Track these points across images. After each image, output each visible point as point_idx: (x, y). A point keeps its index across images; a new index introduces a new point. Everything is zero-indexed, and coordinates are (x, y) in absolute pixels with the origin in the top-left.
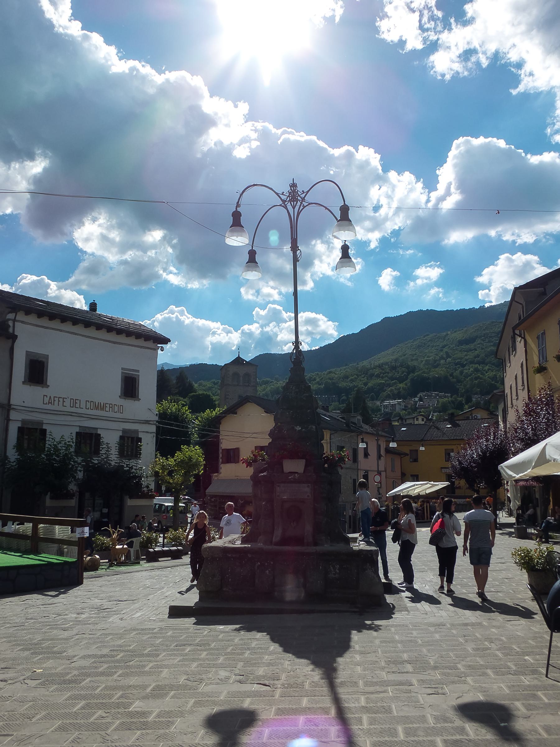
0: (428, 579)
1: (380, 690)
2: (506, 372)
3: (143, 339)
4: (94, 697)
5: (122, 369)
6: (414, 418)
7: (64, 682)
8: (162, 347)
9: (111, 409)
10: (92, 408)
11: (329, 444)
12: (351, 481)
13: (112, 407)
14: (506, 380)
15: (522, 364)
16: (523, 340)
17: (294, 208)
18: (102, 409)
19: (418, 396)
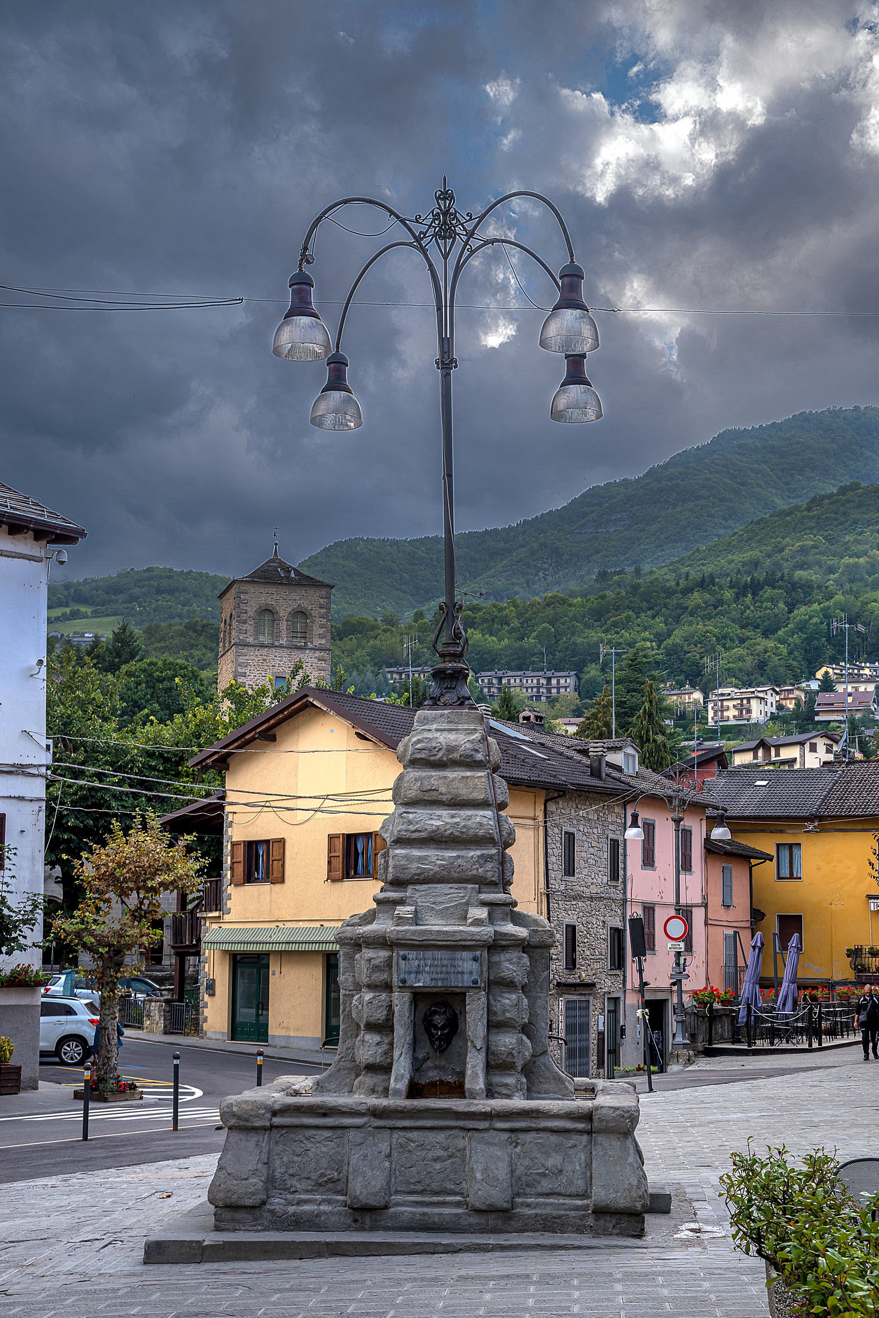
6: (802, 744)
11: (541, 829)
12: (604, 933)
17: (446, 256)
19: (819, 674)
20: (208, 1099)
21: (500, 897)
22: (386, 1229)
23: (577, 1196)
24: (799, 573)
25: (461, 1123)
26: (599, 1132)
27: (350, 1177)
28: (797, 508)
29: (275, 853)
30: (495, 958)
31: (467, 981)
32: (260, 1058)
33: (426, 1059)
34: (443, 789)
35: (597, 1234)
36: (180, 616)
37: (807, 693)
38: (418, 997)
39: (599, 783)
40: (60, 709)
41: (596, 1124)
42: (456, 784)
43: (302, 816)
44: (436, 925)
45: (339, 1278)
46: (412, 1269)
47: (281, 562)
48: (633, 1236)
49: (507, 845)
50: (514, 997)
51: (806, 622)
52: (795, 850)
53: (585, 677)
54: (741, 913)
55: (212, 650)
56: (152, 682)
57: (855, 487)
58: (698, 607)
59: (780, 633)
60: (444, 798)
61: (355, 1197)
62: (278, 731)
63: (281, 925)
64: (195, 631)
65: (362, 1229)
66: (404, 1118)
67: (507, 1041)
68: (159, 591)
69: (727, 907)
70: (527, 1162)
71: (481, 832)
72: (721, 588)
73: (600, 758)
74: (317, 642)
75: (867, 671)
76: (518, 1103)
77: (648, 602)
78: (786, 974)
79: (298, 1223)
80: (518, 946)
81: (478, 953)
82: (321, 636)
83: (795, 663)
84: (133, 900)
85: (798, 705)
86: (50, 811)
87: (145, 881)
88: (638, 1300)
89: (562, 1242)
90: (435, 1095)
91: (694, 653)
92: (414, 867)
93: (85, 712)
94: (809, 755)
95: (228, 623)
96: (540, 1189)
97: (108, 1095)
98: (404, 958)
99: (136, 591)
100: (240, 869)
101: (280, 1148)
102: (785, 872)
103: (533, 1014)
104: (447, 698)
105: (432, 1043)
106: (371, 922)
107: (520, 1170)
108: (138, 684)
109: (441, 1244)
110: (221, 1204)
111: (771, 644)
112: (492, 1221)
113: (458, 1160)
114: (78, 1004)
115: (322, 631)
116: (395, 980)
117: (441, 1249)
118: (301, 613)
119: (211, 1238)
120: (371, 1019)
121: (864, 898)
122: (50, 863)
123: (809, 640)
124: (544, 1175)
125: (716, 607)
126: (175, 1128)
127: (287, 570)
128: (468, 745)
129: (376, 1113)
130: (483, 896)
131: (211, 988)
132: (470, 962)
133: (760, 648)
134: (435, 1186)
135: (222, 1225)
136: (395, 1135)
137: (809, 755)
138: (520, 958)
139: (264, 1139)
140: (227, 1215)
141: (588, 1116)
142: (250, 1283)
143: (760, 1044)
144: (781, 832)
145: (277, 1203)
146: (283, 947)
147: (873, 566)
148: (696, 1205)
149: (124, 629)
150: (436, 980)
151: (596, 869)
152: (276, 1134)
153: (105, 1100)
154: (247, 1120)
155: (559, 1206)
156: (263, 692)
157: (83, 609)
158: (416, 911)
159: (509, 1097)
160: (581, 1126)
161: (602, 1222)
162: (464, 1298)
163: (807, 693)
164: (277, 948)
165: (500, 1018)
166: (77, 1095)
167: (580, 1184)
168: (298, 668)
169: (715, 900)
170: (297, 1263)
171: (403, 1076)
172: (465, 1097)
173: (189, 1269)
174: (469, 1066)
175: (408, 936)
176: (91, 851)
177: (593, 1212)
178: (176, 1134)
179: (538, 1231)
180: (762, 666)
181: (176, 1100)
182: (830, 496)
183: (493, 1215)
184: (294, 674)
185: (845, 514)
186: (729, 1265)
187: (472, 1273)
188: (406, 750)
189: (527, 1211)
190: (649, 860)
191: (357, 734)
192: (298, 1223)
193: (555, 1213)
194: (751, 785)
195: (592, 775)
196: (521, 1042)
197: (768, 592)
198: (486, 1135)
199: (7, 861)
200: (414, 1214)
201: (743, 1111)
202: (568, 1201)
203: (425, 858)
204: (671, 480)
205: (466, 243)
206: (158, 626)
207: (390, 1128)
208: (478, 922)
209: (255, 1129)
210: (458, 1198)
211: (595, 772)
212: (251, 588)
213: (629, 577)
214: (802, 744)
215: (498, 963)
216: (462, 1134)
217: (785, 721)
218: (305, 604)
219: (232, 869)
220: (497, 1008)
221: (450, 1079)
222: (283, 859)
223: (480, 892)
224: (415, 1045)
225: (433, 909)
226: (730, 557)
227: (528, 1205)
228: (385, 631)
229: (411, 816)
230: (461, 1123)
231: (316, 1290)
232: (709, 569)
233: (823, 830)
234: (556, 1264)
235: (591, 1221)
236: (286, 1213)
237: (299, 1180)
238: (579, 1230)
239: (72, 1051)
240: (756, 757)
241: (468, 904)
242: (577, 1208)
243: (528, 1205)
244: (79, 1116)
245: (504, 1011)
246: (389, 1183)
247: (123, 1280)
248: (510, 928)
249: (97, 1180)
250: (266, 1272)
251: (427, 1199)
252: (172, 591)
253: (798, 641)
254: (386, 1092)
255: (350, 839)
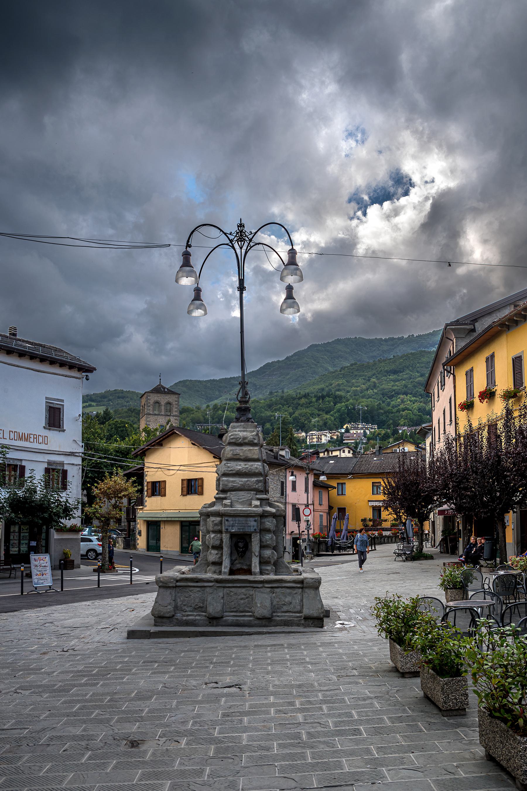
0: (363, 604)
1: (333, 688)
2: (434, 407)
3: (67, 367)
4: (86, 701)
5: (47, 398)
6: (340, 450)
7: (55, 691)
8: (87, 376)
9: (35, 440)
10: (16, 439)
13: (36, 438)
14: (434, 414)
15: (450, 399)
16: (452, 376)
17: (241, 248)
18: (26, 440)
19: (345, 427)
20: (141, 572)
21: (264, 496)
22: (222, 626)
23: (297, 612)
24: (337, 393)
25: (251, 585)
26: (306, 588)
27: (208, 606)
28: (336, 371)
29: (162, 485)
30: (263, 521)
31: (252, 529)
32: (161, 558)
33: (235, 560)
34: (241, 454)
35: (305, 626)
36: (126, 406)
37: (340, 433)
38: (233, 536)
39: (278, 462)
40: (86, 435)
41: (305, 585)
42: (247, 452)
43: (172, 472)
44: (239, 508)
45: (206, 646)
46: (235, 642)
47: (162, 386)
48: (320, 627)
49: (267, 476)
50: (270, 535)
51: (340, 409)
52: (344, 486)
53: (265, 428)
54: (325, 507)
55: (137, 418)
56: (117, 428)
57: (355, 364)
58: (304, 404)
59: (331, 413)
60: (242, 458)
61: (210, 614)
62: (163, 442)
63: (165, 511)
64: (131, 411)
65: (213, 626)
66: (229, 583)
67: (268, 553)
68: (119, 397)
69: (320, 505)
70: (278, 600)
71: (257, 471)
72: (311, 397)
73: (277, 453)
74: (175, 413)
75: (360, 426)
76: (272, 577)
77: (287, 402)
78: (344, 528)
79: (187, 623)
80: (272, 516)
81: (256, 518)
82: (176, 411)
83: (336, 423)
84: (113, 501)
85: (338, 437)
86: (83, 470)
87: (117, 494)
88: (332, 655)
89: (293, 630)
90: (239, 574)
91: (303, 420)
92: (230, 485)
93: (94, 436)
94: (342, 454)
95: (144, 407)
96: (282, 610)
97: (105, 571)
98: (227, 520)
99: (111, 397)
100: (150, 491)
101: (179, 594)
102: (340, 493)
103: (277, 542)
104: (242, 418)
105: (238, 554)
106: (213, 507)
107: (275, 603)
108: (112, 428)
109: (245, 632)
110: (156, 616)
111: (328, 416)
112: (264, 622)
113: (250, 599)
114: (94, 538)
115: (176, 410)
116: (223, 529)
117: (245, 633)
118: (169, 403)
119: (153, 629)
120: (214, 544)
121: (367, 501)
122: (83, 489)
123: (341, 415)
124: (284, 605)
125: (310, 404)
126: (131, 583)
127: (164, 388)
128: (251, 437)
129: (217, 581)
130: (258, 496)
131: (140, 533)
132: (253, 522)
133: (324, 418)
134: (241, 609)
135: (157, 624)
136: (225, 590)
137: (342, 454)
138: (272, 520)
139: (173, 591)
140: (159, 620)
141: (302, 582)
142: (171, 647)
143: (336, 552)
144: (339, 479)
145: (179, 616)
146: (166, 519)
147: (362, 390)
148: (339, 613)
149: (107, 410)
150: (240, 529)
151: (276, 492)
152: (178, 589)
153: (104, 572)
154: (166, 584)
155: (290, 616)
156: (156, 430)
157: (93, 404)
158: (231, 502)
159: (268, 574)
160: (299, 585)
161: (307, 622)
162: (260, 655)
163: (340, 433)
164: (163, 519)
165: (265, 544)
166: (95, 570)
167: (298, 608)
168: (169, 421)
169: (317, 502)
170: (188, 639)
171: (227, 566)
172: (252, 575)
173: (146, 641)
174: (253, 563)
175: (229, 512)
176: (98, 483)
177: (304, 618)
178: (132, 585)
179: (282, 626)
180: (325, 424)
181: (131, 572)
182: (347, 367)
183: (265, 620)
184: (168, 423)
185: (352, 373)
186: (361, 638)
187: (259, 643)
188: (226, 439)
189: (278, 619)
190: (294, 489)
191: (192, 443)
192: (187, 623)
193: (289, 619)
194: (328, 462)
195: (275, 458)
196: (273, 553)
197: (327, 399)
198: (261, 589)
199: (68, 487)
200: (233, 620)
201: (339, 576)
202: (294, 614)
203: (235, 481)
204: (294, 361)
205: (249, 244)
206: (118, 410)
207: (223, 587)
208: (256, 506)
209: (169, 587)
210: (250, 614)
211: (276, 457)
212: (151, 395)
213: (280, 394)
214: (340, 450)
215: (264, 523)
216: (252, 589)
217: (333, 442)
218: (171, 400)
219: (147, 491)
220: (264, 540)
221: (245, 567)
222: (165, 488)
223: (256, 495)
224: (231, 554)
225: (238, 501)
226: (314, 387)
227: (278, 616)
228: (196, 411)
229: (229, 465)
230: (251, 585)
231: (198, 651)
232: (307, 391)
233: (354, 478)
234: (292, 639)
235: (303, 622)
236: (182, 619)
237: (188, 607)
238: (298, 625)
239: (92, 554)
240: (324, 455)
241: (252, 499)
242: (297, 617)
243: (278, 616)
244: (96, 578)
245: (267, 541)
246: (223, 608)
247: (120, 646)
248: (268, 509)
249: (105, 603)
250: (176, 643)
251: (238, 614)
252: (123, 398)
253: (337, 416)
254: (220, 573)
255: (189, 481)
